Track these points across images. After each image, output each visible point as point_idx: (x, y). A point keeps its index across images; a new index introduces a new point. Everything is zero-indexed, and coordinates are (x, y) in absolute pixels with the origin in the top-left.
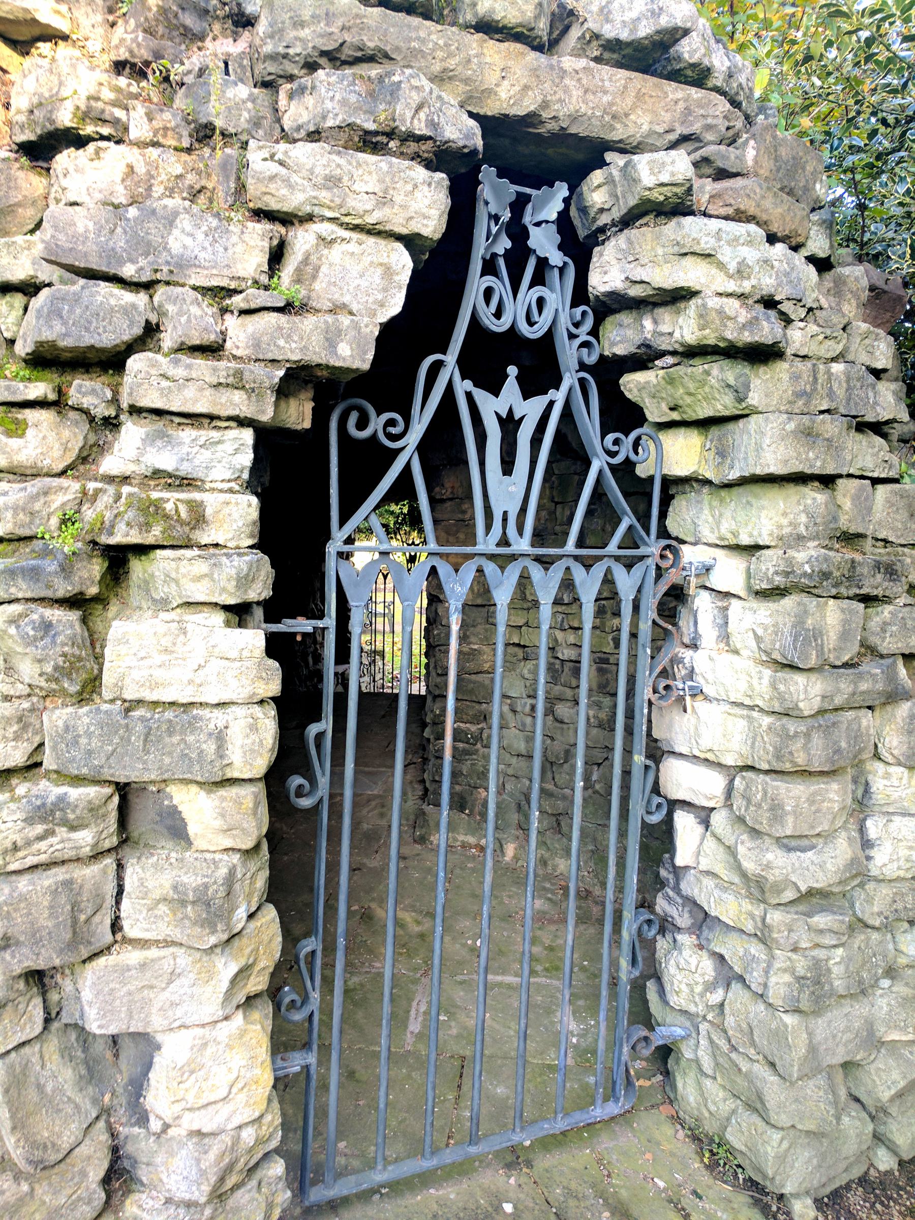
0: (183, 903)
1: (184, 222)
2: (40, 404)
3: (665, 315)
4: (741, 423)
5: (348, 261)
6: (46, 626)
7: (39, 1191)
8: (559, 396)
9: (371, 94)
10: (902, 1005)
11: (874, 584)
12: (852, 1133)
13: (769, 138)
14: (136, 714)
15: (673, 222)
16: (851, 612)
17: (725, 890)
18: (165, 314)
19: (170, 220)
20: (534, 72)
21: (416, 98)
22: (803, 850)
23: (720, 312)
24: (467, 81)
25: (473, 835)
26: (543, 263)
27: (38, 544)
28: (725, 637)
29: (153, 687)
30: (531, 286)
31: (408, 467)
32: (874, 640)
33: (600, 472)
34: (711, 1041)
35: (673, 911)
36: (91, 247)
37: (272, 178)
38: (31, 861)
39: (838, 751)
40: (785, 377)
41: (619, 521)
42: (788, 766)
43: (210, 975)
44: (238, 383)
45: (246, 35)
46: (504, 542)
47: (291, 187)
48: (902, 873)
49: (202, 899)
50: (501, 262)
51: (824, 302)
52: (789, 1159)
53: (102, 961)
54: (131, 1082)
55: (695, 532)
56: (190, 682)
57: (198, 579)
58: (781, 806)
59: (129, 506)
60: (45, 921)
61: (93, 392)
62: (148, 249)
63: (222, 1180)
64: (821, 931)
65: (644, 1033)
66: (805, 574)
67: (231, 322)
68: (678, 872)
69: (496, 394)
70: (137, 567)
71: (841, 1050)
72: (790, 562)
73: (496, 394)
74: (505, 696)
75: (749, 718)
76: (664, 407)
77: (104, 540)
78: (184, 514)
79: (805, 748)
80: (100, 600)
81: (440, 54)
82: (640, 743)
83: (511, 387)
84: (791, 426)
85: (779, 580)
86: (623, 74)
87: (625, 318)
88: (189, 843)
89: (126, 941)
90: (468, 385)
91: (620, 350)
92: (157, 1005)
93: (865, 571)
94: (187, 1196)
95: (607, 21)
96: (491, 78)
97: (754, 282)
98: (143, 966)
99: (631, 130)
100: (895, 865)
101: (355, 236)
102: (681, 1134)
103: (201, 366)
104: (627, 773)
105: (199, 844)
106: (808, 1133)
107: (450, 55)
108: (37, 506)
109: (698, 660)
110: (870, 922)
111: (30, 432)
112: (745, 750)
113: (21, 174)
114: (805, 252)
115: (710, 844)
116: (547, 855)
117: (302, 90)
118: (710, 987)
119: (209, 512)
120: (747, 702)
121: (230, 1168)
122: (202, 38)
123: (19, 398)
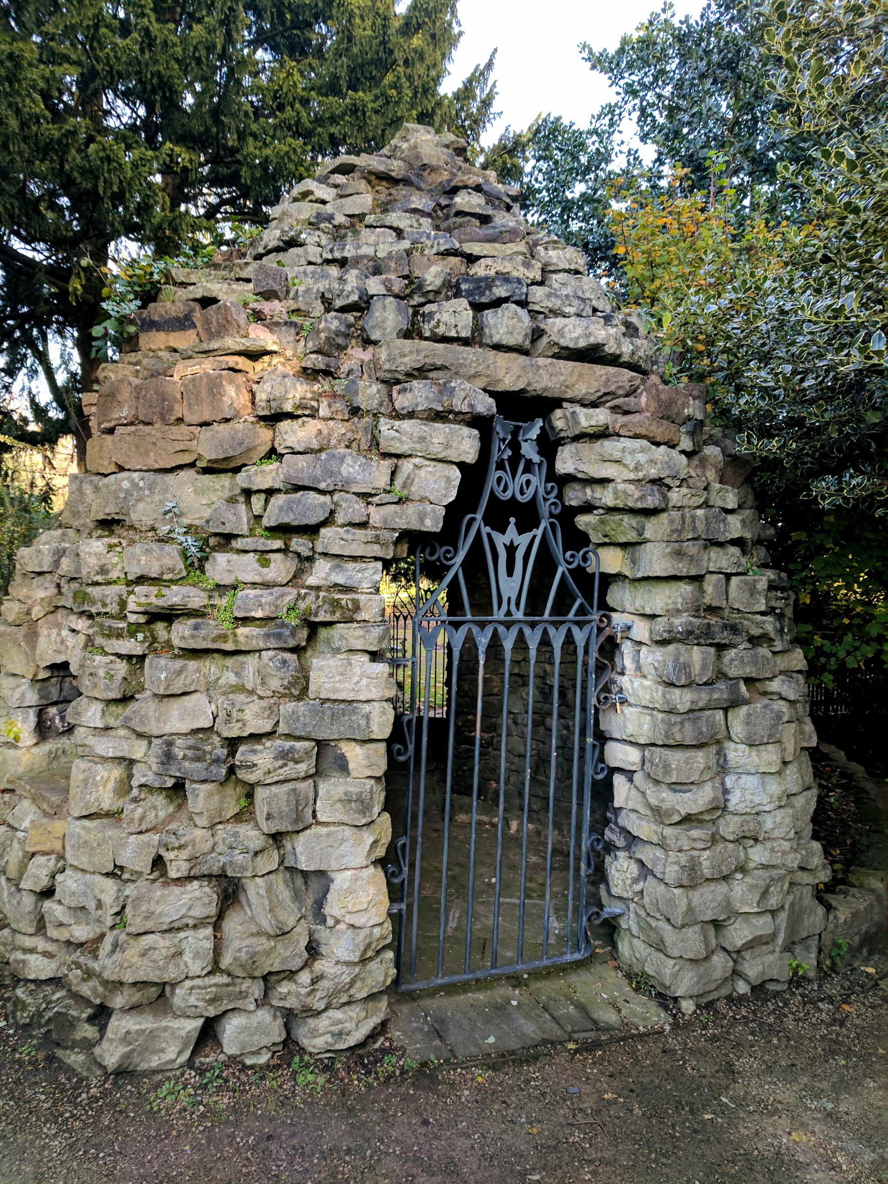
0: (350, 801)
1: (349, 460)
2: (278, 551)
3: (598, 489)
4: (643, 546)
5: (428, 476)
6: (284, 662)
7: (278, 947)
8: (539, 532)
9: (440, 392)
10: (750, 890)
11: (722, 637)
12: (719, 965)
13: (654, 391)
14: (326, 705)
15: (599, 443)
16: (707, 653)
17: (641, 819)
18: (340, 506)
19: (342, 459)
20: (524, 368)
21: (463, 394)
22: (684, 792)
23: (625, 492)
24: (488, 376)
25: (487, 815)
26: (529, 463)
27: (279, 621)
28: (639, 668)
29: (335, 691)
30: (523, 473)
31: (456, 576)
32: (726, 669)
33: (563, 574)
34: (636, 913)
35: (614, 837)
36: (305, 475)
37: (393, 439)
38: (276, 779)
39: (701, 733)
40: (666, 522)
41: (575, 600)
42: (672, 742)
43: (360, 842)
44: (377, 540)
45: (370, 349)
46: (509, 613)
47: (401, 442)
48: (748, 810)
49: (360, 800)
50: (506, 463)
51: (693, 474)
52: (679, 977)
53: (308, 831)
54: (316, 902)
55: (622, 605)
56: (353, 689)
57: (358, 638)
58: (669, 765)
59: (324, 602)
60: (285, 809)
61: (304, 544)
62: (331, 474)
63: (365, 951)
64: (695, 840)
65: (596, 910)
66: (679, 632)
67: (372, 509)
68: (617, 811)
69: (504, 533)
70: (323, 633)
71: (709, 912)
72: (671, 625)
73: (504, 533)
74: (510, 712)
75: (652, 715)
76: (600, 535)
77: (313, 619)
78: (350, 606)
79: (680, 730)
80: (304, 649)
81: (474, 365)
82: (590, 731)
83: (512, 529)
84: (668, 550)
85: (665, 635)
86: (571, 364)
87: (577, 486)
88: (349, 774)
89: (318, 823)
90: (488, 529)
91: (574, 503)
92: (334, 856)
93: (717, 629)
94: (348, 959)
95: (562, 337)
96: (500, 374)
97: (644, 472)
98: (328, 835)
99: (576, 393)
100: (744, 804)
101: (433, 463)
102: (620, 974)
103: (360, 533)
104: (582, 749)
105: (354, 774)
106: (691, 960)
107: (479, 364)
108: (279, 602)
109: (624, 681)
110: (728, 838)
111: (272, 565)
112: (650, 734)
113: (260, 430)
114: (679, 448)
115: (634, 792)
116: (540, 828)
117: (405, 390)
118: (635, 881)
119: (362, 604)
120: (651, 706)
121: (370, 944)
122: (346, 348)
123: (268, 549)
